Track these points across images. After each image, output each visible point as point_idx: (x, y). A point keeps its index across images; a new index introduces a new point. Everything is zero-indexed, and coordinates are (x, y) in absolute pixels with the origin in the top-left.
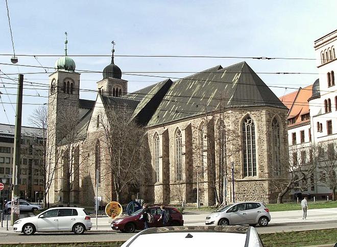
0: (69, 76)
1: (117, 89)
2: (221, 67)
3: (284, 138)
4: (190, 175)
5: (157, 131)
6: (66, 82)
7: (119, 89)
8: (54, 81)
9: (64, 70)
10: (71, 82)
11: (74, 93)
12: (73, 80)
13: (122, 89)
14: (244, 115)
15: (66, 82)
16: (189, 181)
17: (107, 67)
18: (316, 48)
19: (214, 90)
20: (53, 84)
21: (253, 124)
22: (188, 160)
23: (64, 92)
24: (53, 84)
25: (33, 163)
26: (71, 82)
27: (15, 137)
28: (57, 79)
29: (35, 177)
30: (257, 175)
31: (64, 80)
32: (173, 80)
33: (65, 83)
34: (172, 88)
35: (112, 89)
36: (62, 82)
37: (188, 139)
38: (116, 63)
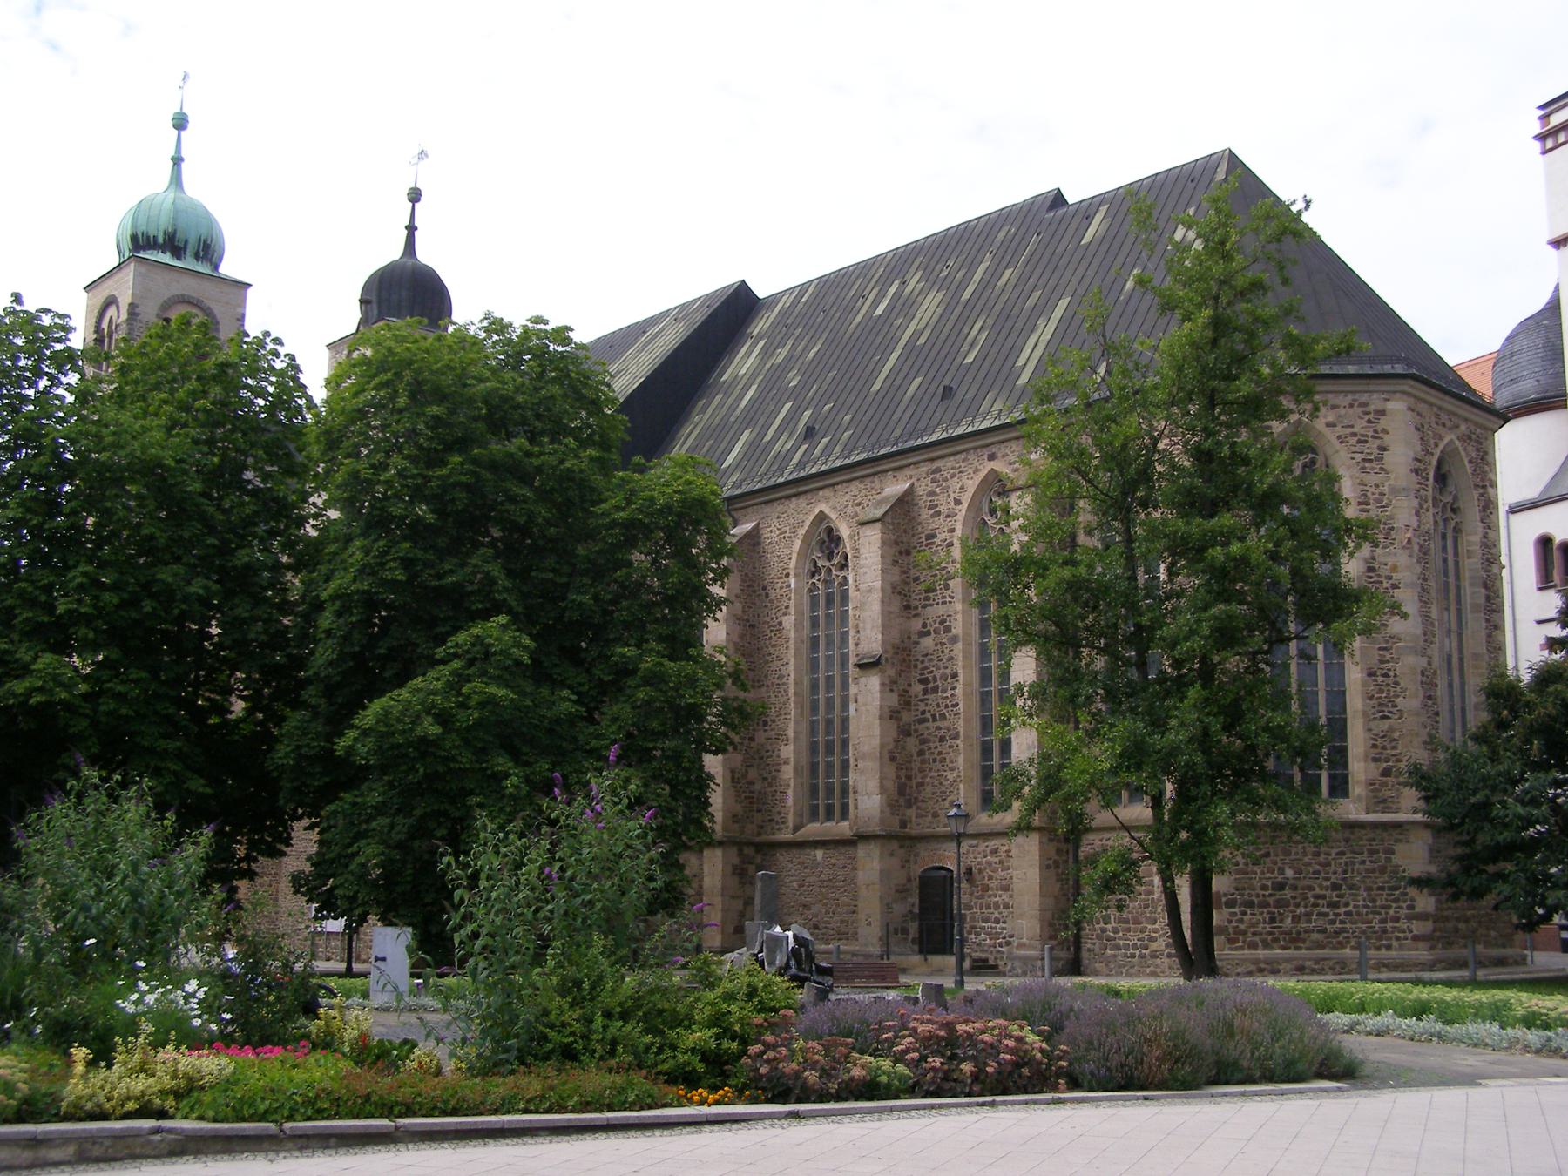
0: (189, 287)
2: (1058, 199)
3: (1486, 586)
4: (902, 790)
5: (827, 511)
6: (175, 315)
8: (112, 312)
9: (166, 258)
12: (208, 312)
15: (175, 315)
16: (896, 821)
17: (367, 288)
18: (1550, 143)
19: (1043, 309)
20: (105, 325)
22: (893, 700)
24: (105, 325)
25: (1481, 491)
27: (885, 961)
28: (125, 300)
30: (1357, 790)
31: (167, 305)
32: (761, 290)
34: (760, 325)
36: (150, 313)
37: (896, 577)
38: (426, 255)
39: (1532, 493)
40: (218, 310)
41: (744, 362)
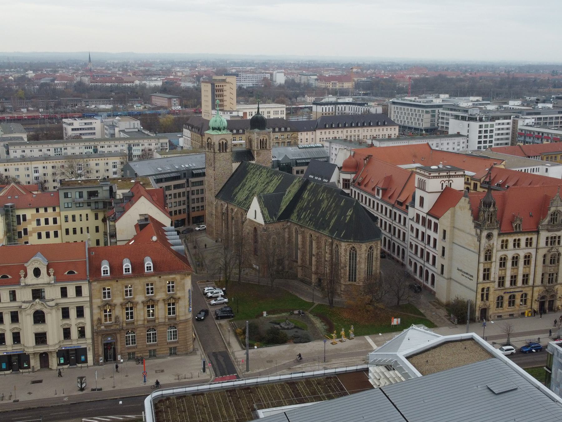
0: (223, 137)
1: (263, 139)
6: (221, 142)
7: (265, 139)
10: (224, 142)
11: (228, 150)
12: (226, 140)
13: (268, 139)
14: (351, 246)
21: (356, 251)
23: (220, 152)
26: (224, 142)
29: (193, 205)
31: (219, 141)
33: (220, 143)
35: (259, 140)
39: (411, 218)
40: (228, 139)
41: (305, 195)
